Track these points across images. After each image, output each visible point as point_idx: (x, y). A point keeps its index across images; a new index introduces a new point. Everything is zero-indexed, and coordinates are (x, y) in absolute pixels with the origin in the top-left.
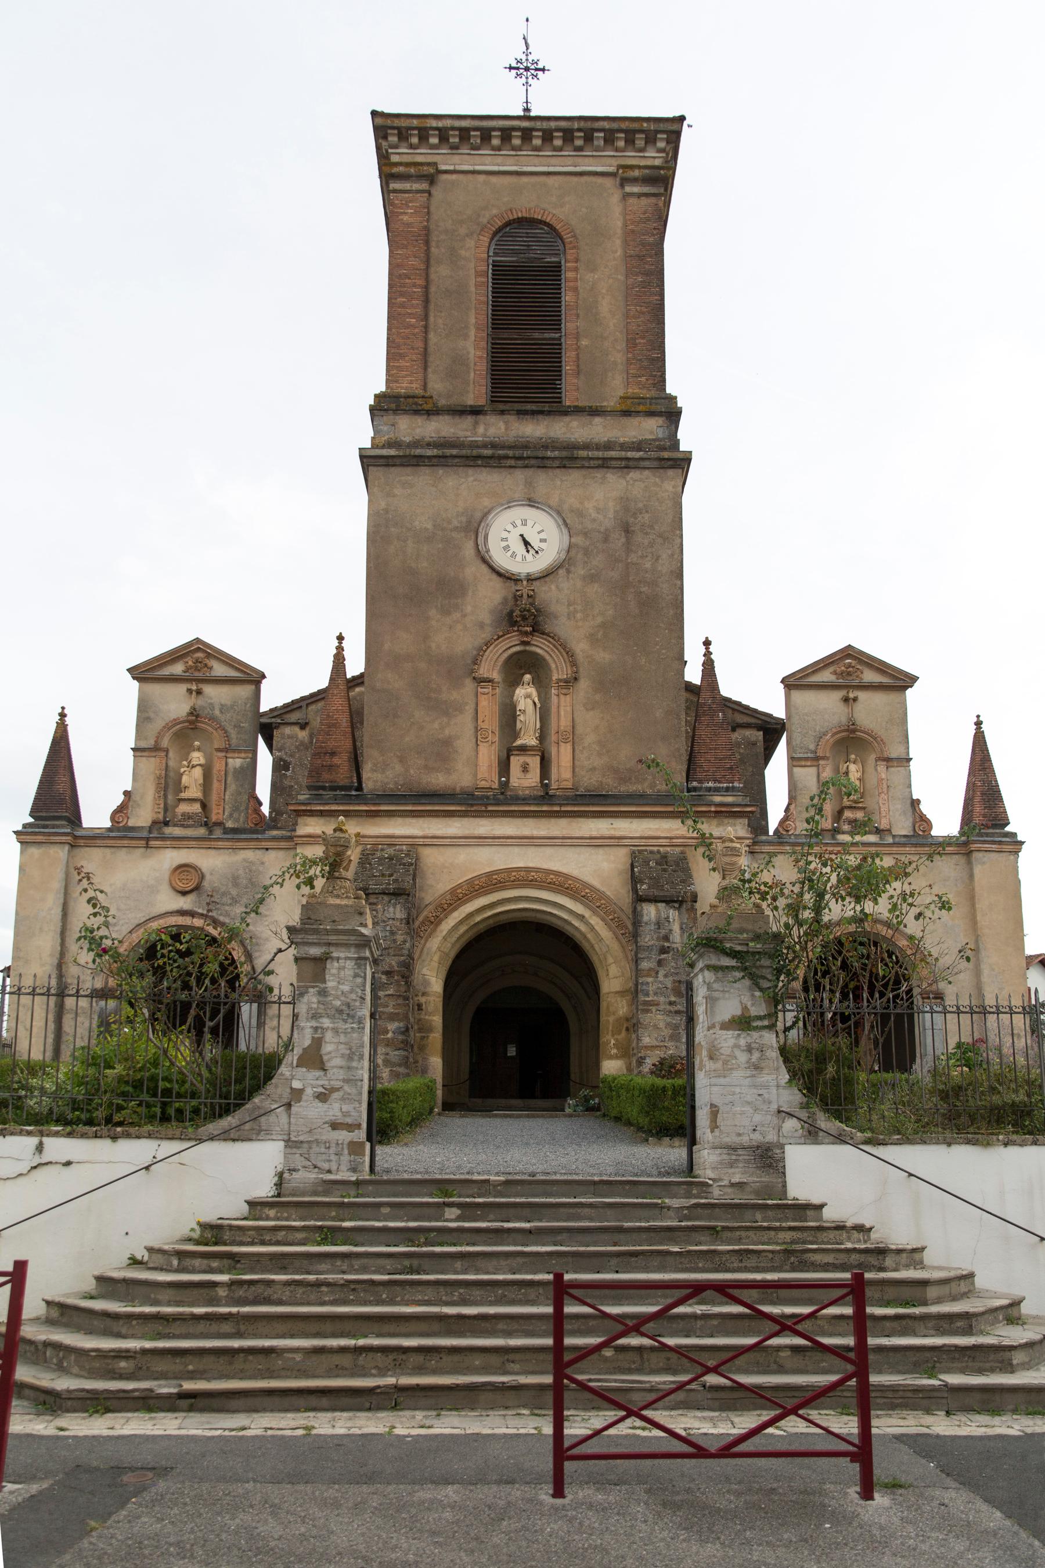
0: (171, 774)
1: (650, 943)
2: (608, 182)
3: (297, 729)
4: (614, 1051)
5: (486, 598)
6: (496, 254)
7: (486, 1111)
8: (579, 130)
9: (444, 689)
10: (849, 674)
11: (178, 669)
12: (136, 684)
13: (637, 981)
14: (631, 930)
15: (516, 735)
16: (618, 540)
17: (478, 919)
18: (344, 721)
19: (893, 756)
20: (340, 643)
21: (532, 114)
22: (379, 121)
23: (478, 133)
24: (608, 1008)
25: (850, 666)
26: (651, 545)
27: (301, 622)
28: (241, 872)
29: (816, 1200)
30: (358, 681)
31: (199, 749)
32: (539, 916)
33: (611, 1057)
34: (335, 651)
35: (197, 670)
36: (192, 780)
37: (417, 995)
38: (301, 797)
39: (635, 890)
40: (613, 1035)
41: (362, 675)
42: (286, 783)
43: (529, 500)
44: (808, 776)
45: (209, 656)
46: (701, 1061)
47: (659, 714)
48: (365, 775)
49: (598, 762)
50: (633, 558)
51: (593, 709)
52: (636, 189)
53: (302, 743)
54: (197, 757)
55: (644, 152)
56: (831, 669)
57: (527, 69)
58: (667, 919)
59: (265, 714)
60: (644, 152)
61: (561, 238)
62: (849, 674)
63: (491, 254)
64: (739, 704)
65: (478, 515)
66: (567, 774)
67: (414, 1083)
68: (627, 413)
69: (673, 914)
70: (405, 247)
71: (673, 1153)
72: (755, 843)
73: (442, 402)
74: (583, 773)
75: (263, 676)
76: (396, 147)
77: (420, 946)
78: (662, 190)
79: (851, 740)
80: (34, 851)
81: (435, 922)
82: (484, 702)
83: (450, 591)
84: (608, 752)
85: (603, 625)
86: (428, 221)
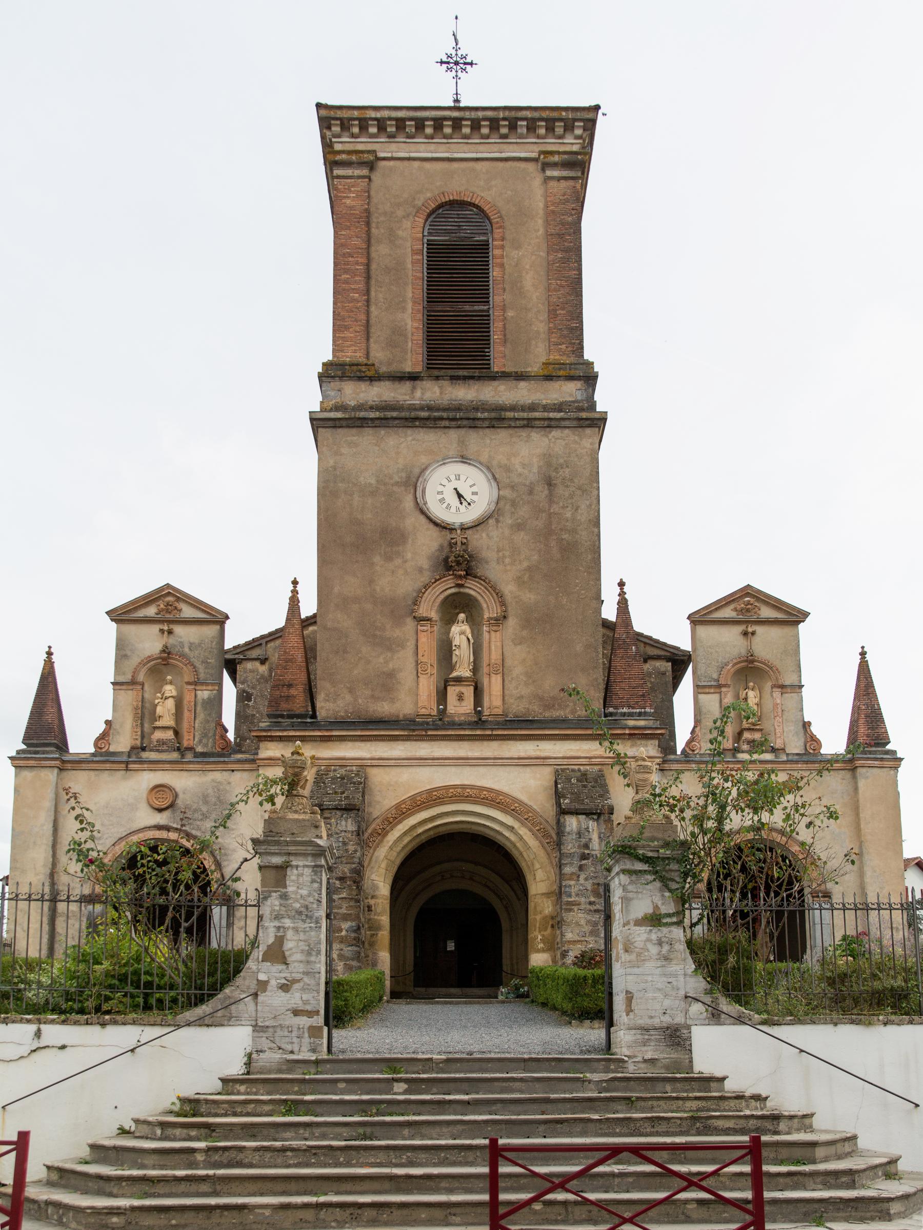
0: (147, 705)
1: (572, 851)
2: (531, 167)
3: (257, 664)
4: (541, 946)
5: (425, 546)
6: (430, 234)
7: (428, 998)
8: (504, 119)
9: (388, 626)
10: (748, 610)
11: (151, 611)
12: (114, 625)
13: (561, 884)
14: (555, 840)
15: (452, 668)
16: (542, 493)
17: (420, 830)
18: (299, 656)
19: (787, 683)
20: (295, 587)
21: (462, 105)
22: (324, 113)
23: (413, 123)
24: (535, 907)
25: (749, 603)
26: (571, 496)
27: (260, 570)
28: (210, 791)
29: (719, 1074)
30: (311, 621)
31: (171, 683)
32: (474, 827)
33: (538, 951)
34: (290, 595)
35: (168, 612)
36: (165, 710)
37: (367, 898)
38: (262, 725)
39: (558, 804)
40: (540, 932)
41: (315, 616)
42: (249, 712)
43: (462, 457)
44: (711, 702)
45: (178, 599)
46: (618, 953)
47: (579, 648)
48: (319, 704)
49: (525, 691)
50: (555, 508)
51: (520, 644)
52: (556, 173)
53: (262, 677)
54: (170, 690)
55: (563, 138)
56: (732, 606)
57: (457, 63)
58: (587, 829)
59: (229, 651)
60: (563, 138)
61: (489, 219)
62: (748, 610)
63: (426, 234)
64: (650, 638)
65: (417, 471)
66: (497, 702)
67: (365, 974)
68: (549, 378)
69: (592, 825)
70: (348, 228)
71: (594, 1034)
72: (664, 762)
73: (383, 369)
74: (512, 701)
75: (227, 617)
76: (339, 136)
77: (369, 855)
78: (579, 174)
79: (750, 670)
80: (27, 774)
81: (383, 833)
82: (423, 639)
83: (392, 539)
84: (534, 682)
85: (529, 569)
86: (368, 204)
